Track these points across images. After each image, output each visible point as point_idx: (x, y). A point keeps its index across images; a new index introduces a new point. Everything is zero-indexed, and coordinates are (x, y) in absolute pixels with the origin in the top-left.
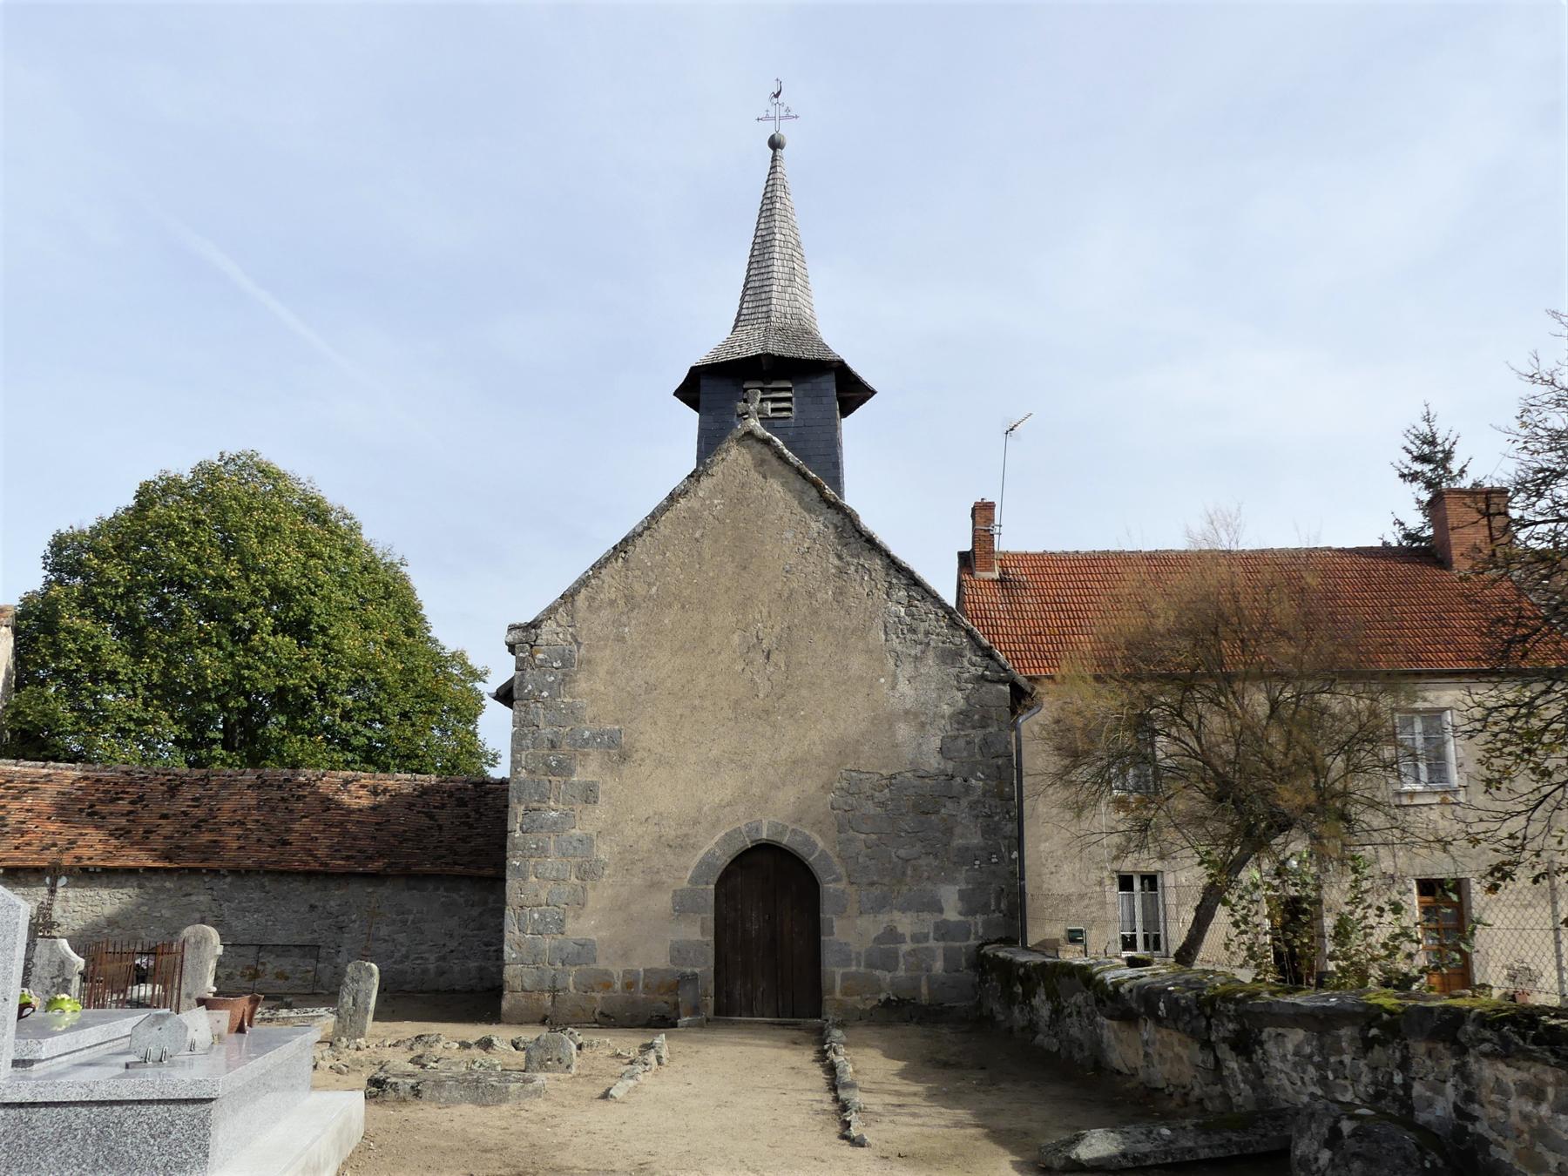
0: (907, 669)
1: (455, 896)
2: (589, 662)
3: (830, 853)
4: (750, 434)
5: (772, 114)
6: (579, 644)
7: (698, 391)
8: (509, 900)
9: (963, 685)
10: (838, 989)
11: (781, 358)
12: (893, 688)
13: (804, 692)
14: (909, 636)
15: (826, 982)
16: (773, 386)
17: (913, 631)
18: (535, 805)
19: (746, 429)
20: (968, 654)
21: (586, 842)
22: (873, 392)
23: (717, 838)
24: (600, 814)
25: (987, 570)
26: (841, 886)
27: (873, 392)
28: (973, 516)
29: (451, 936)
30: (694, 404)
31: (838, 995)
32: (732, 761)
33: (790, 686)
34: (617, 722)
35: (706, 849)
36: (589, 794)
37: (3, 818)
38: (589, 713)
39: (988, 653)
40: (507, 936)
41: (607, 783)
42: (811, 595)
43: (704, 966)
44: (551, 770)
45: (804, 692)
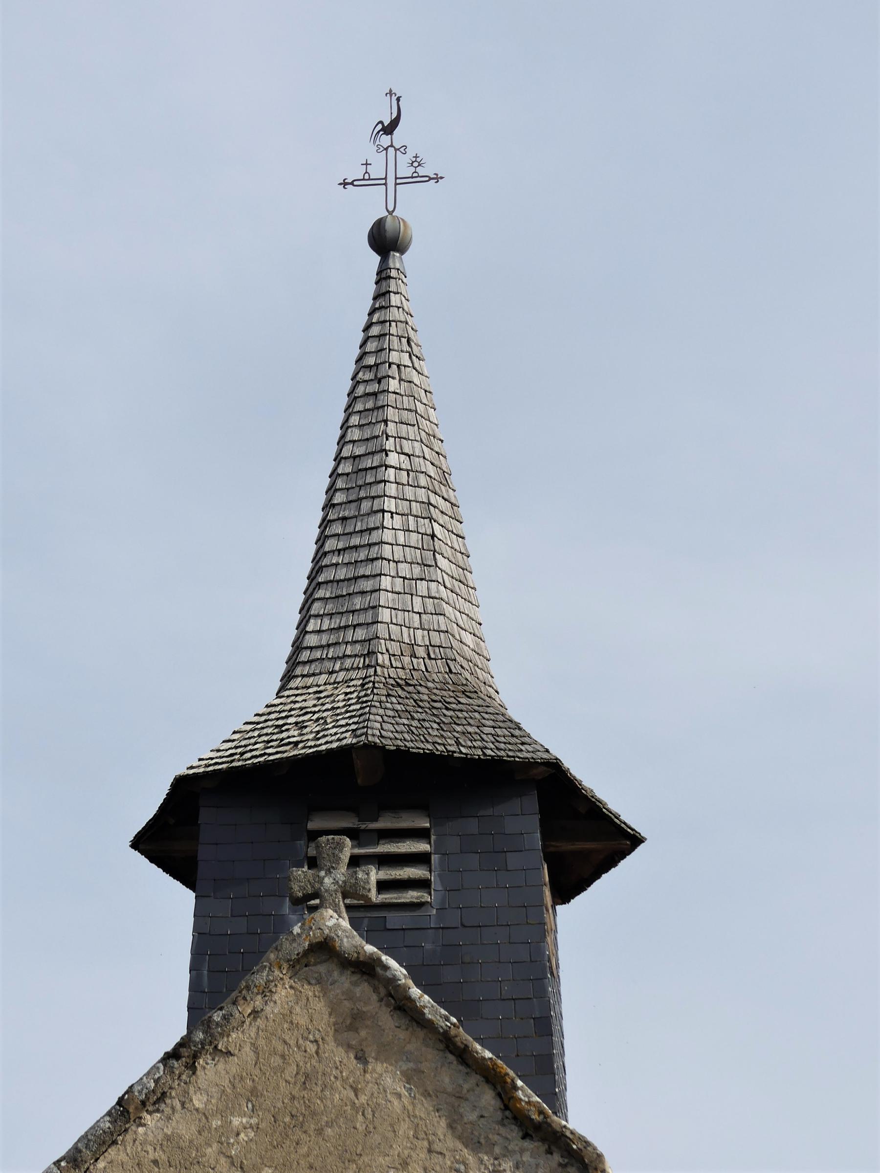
4: (324, 948)
5: (376, 171)
19: (315, 936)
30: (181, 868)
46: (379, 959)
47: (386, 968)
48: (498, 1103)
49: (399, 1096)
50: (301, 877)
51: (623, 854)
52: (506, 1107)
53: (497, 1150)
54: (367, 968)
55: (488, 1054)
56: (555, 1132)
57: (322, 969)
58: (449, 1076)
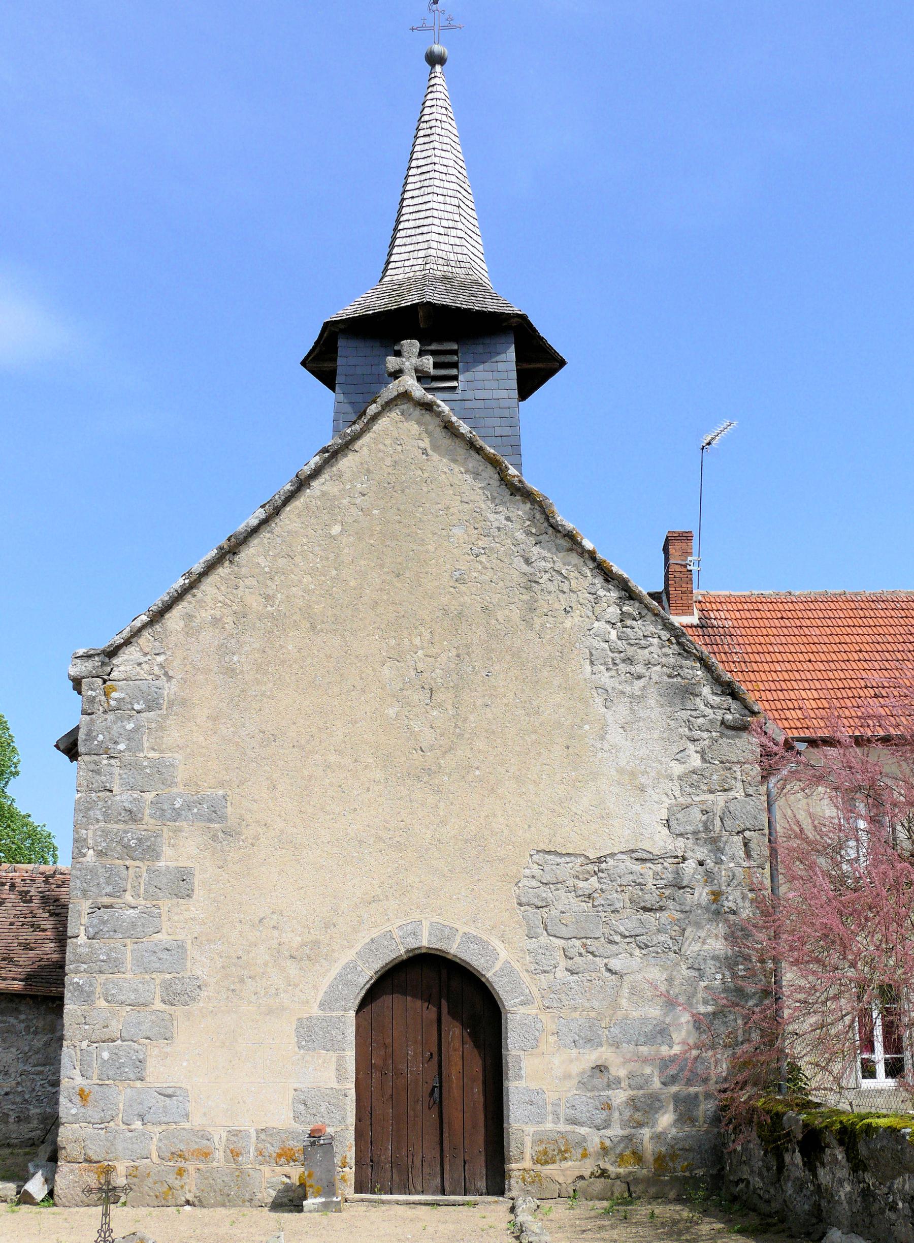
0: (622, 710)
1: (12, 1020)
2: (184, 702)
3: (517, 966)
4: (405, 396)
5: (429, 23)
6: (170, 678)
7: (335, 360)
8: (67, 1033)
9: (697, 734)
10: (528, 1156)
11: (445, 307)
12: (602, 738)
13: (480, 744)
14: (622, 667)
15: (513, 1149)
16: (433, 347)
17: (629, 661)
18: (106, 900)
19: (402, 390)
20: (706, 691)
21: (178, 950)
22: (562, 363)
23: (359, 946)
24: (196, 908)
25: (683, 613)
26: (531, 1010)
27: (562, 363)
28: (666, 549)
29: (6, 1073)
30: (328, 379)
31: (527, 1164)
32: (380, 839)
33: (461, 735)
34: (221, 784)
35: (343, 961)
36: (181, 884)
37: (912, 856)
38: (181, 775)
39: (730, 691)
40: (65, 1082)
41: (204, 874)
42: (182, 1187)
43: (343, 1126)
44: (128, 851)
45: (480, 744)
46: (435, 402)
47: (439, 406)
48: (496, 476)
49: (445, 473)
50: (392, 362)
51: (552, 372)
52: (502, 479)
53: (497, 501)
54: (428, 407)
55: (492, 451)
56: (528, 492)
57: (405, 407)
58: (474, 461)
